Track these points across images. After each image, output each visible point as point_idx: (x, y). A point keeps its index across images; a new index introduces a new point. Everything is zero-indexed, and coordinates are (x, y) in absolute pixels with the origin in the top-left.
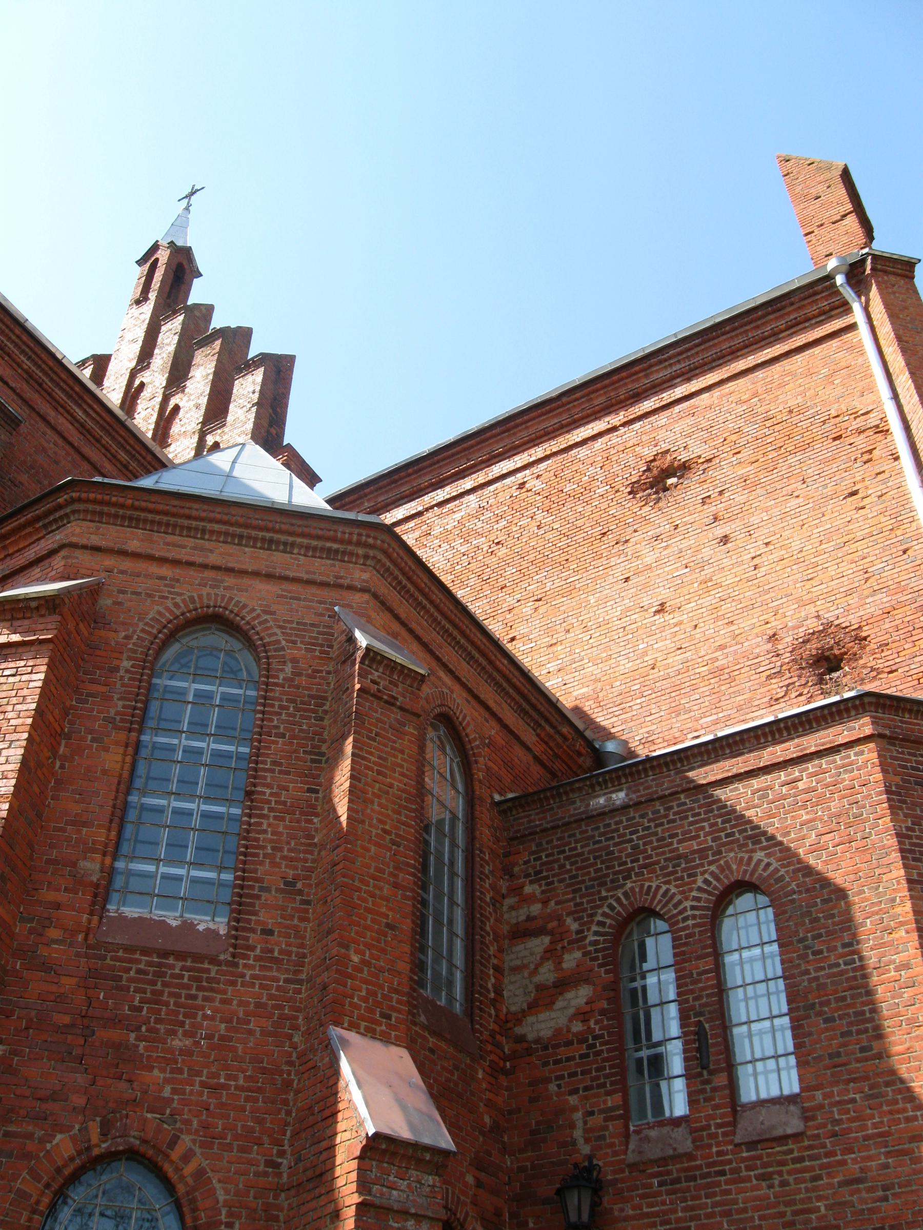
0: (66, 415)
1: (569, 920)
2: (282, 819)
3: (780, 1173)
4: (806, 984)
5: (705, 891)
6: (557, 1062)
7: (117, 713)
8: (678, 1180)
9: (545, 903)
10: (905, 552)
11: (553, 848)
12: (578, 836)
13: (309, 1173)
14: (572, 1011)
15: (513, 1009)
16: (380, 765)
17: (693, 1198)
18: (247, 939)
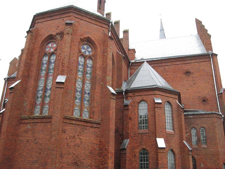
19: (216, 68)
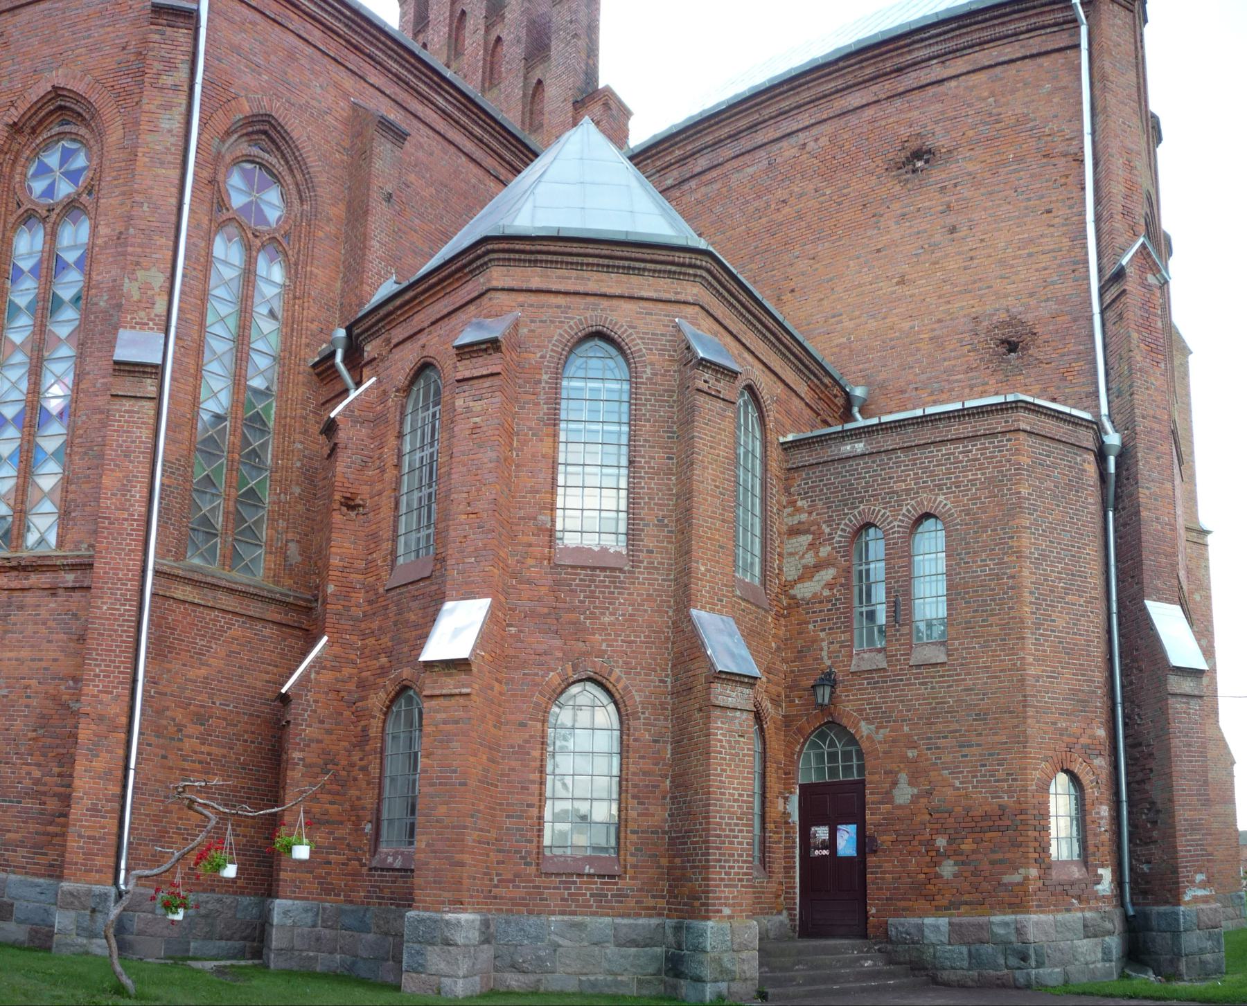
0: (430, 105)
1: (824, 526)
2: (653, 478)
3: (932, 683)
5: (907, 516)
6: (814, 612)
7: (545, 414)
8: (877, 682)
9: (810, 513)
10: (1073, 271)
11: (816, 477)
12: (832, 471)
13: (684, 687)
14: (824, 582)
15: (789, 579)
16: (712, 442)
17: (885, 692)
18: (639, 556)
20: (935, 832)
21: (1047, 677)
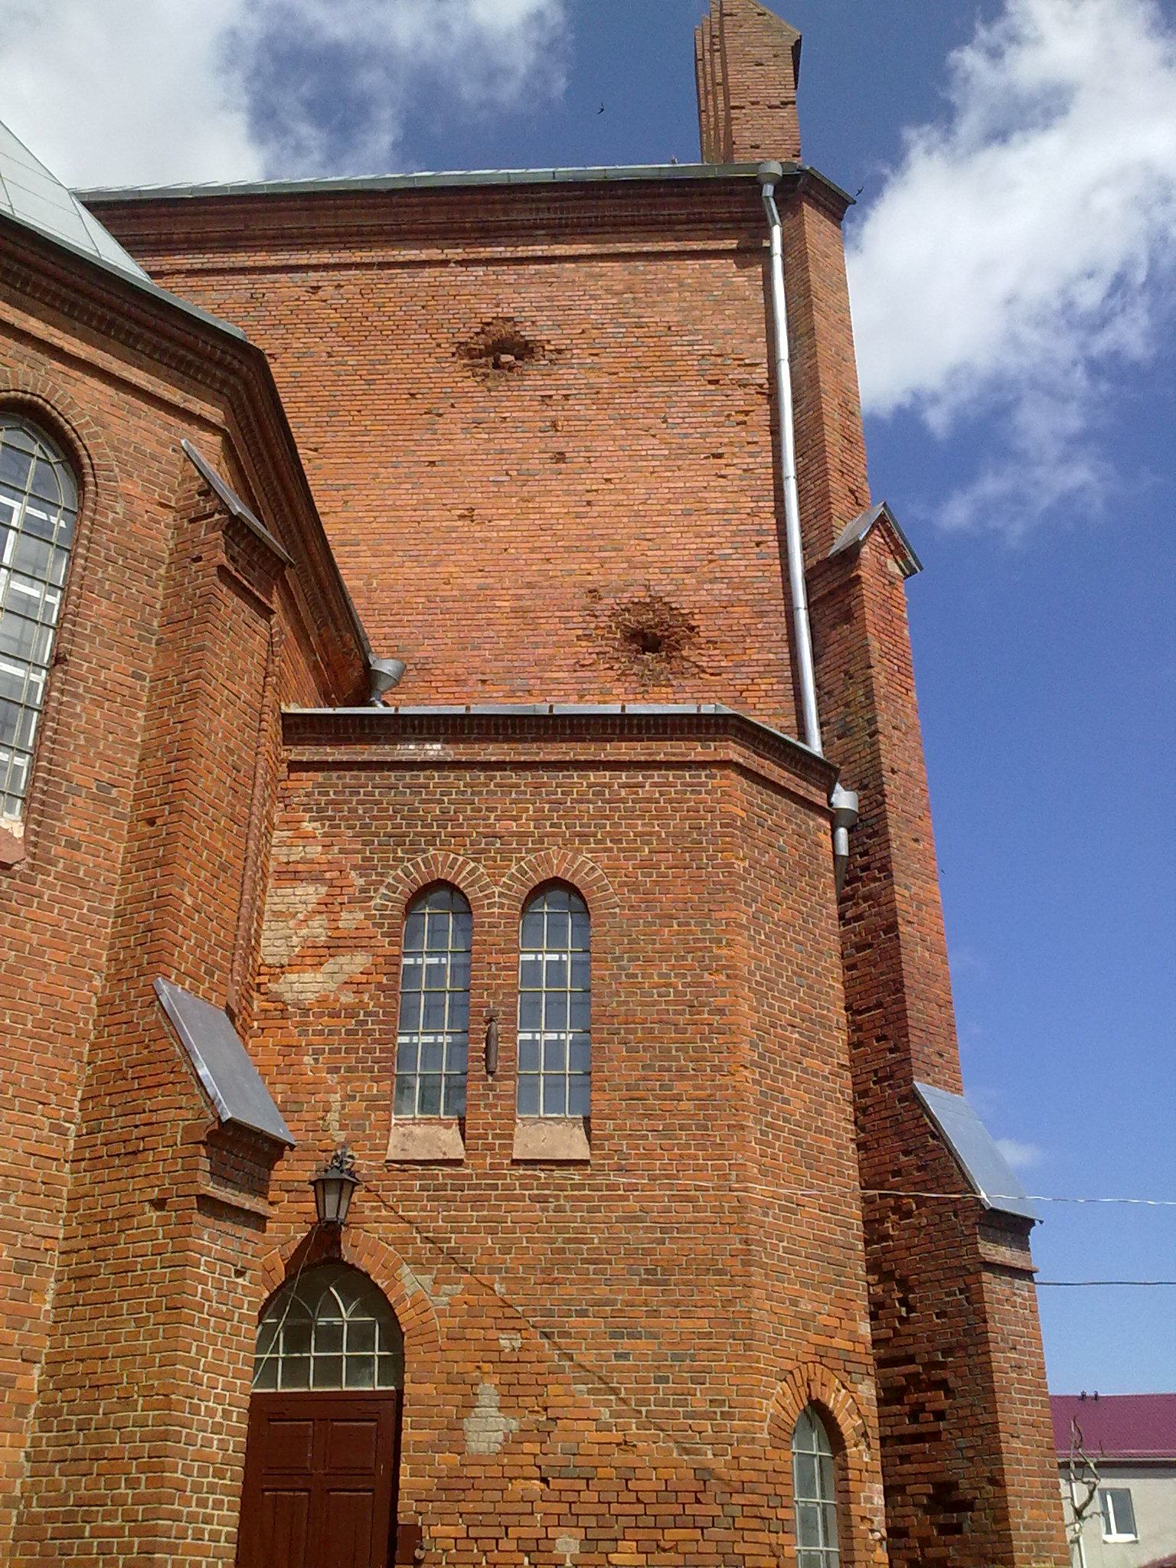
4: (615, 1005)
10: (758, 544)
14: (345, 978)
19: (809, 306)
20: (554, 1520)
21: (782, 1208)
